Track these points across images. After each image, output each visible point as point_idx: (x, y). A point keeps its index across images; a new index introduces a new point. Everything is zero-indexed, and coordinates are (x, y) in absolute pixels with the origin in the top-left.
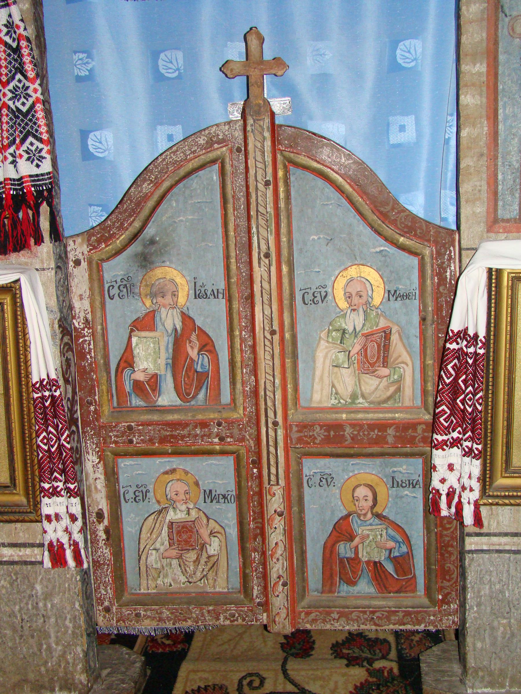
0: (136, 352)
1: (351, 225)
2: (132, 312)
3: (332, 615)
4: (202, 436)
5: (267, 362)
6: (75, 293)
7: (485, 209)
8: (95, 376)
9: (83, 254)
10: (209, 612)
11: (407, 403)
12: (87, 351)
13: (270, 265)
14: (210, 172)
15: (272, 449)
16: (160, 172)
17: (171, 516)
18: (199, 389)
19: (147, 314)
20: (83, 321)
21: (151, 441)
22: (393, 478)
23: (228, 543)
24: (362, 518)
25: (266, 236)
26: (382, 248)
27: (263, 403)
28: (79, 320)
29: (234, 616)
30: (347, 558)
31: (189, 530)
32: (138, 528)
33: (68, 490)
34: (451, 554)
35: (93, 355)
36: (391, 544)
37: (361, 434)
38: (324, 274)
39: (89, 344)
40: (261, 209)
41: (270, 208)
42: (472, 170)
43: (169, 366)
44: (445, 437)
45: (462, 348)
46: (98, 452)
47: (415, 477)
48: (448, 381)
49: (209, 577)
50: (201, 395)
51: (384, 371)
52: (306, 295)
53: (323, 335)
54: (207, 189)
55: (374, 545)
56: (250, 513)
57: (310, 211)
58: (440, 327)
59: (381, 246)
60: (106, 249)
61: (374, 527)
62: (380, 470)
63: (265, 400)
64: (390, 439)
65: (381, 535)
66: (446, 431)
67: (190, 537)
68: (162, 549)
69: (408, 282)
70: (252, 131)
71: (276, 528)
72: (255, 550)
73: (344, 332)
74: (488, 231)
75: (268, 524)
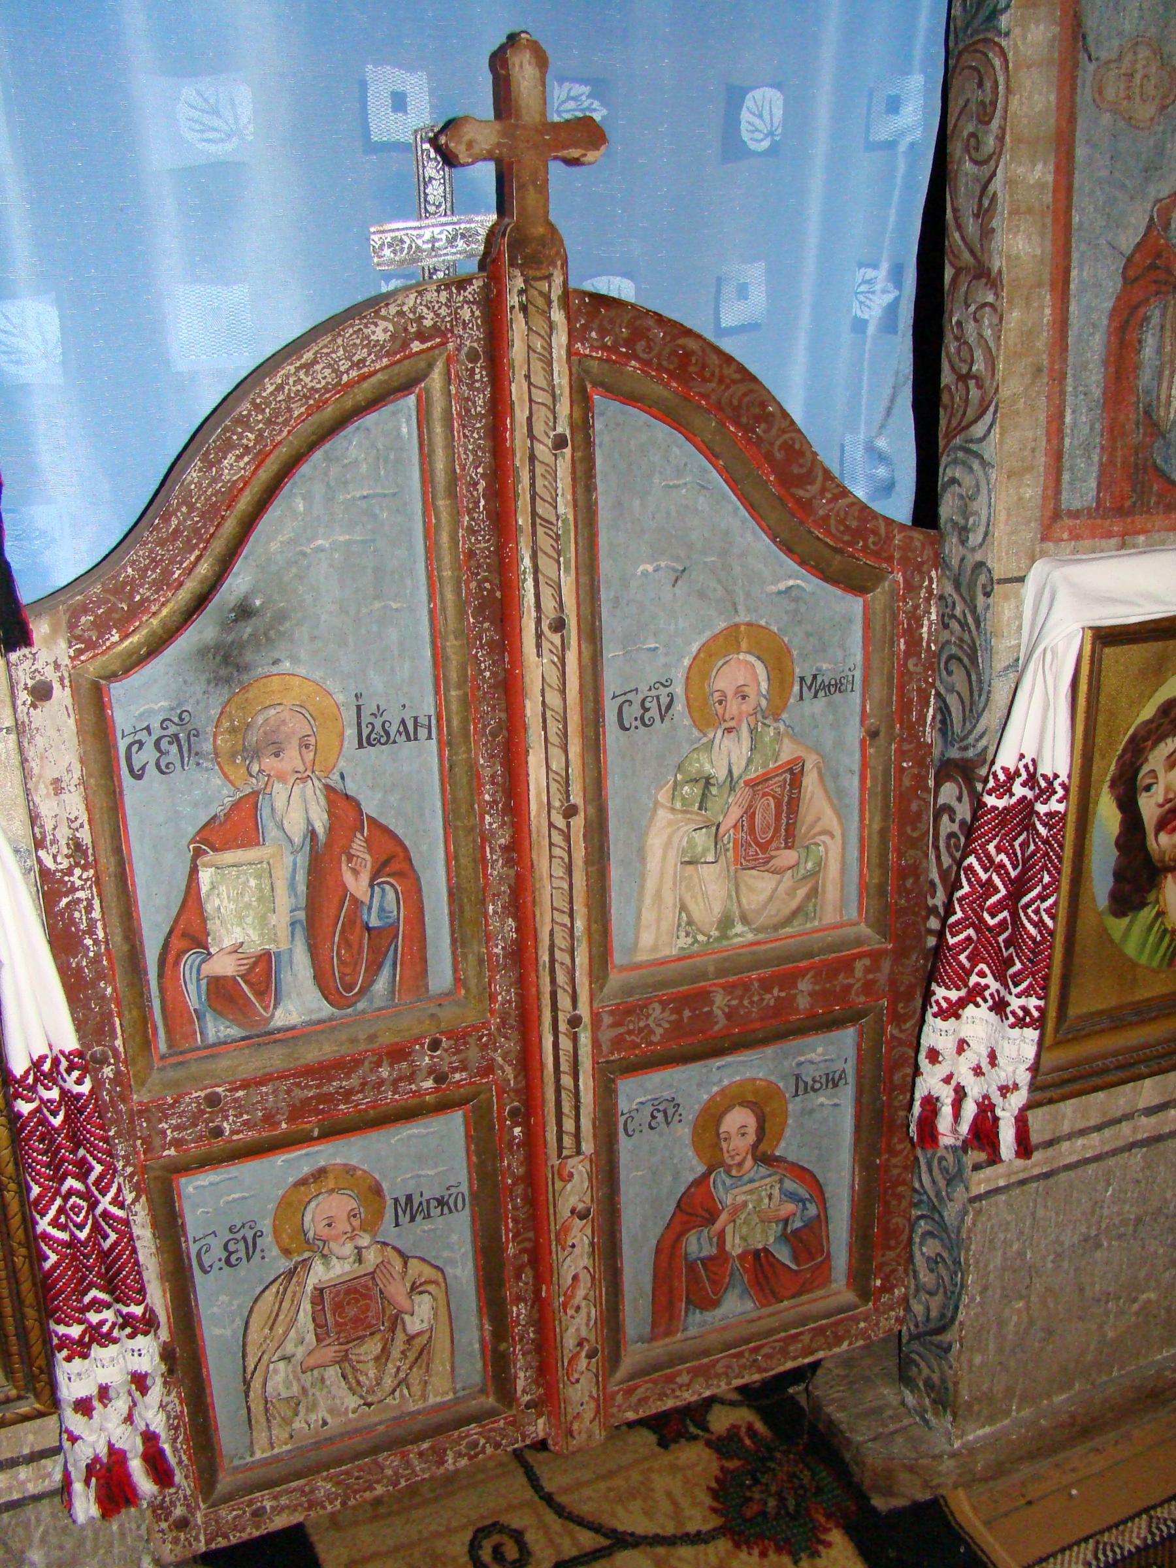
0: (209, 908)
1: (727, 533)
2: (195, 805)
3: (679, 1380)
4: (395, 1083)
5: (556, 883)
6: (40, 776)
7: (1039, 490)
8: (109, 990)
9: (57, 666)
10: (421, 1454)
12: (83, 927)
13: (563, 650)
14: (394, 414)
15: (567, 1081)
16: (269, 422)
17: (319, 1274)
18: (375, 968)
19: (236, 805)
20: (66, 851)
21: (269, 1119)
23: (451, 1297)
24: (734, 1173)
25: (554, 577)
26: (791, 583)
27: (548, 980)
28: (54, 850)
29: (476, 1444)
30: (702, 1260)
31: (362, 1295)
32: (239, 1323)
33: (127, 1320)
35: (101, 934)
37: (746, 1002)
38: (666, 654)
39: (89, 908)
42: (1021, 404)
43: (298, 927)
46: (132, 1175)
49: (411, 1381)
50: (381, 984)
51: (788, 857)
52: (626, 707)
53: (663, 796)
54: (386, 461)
56: (507, 1225)
57: (637, 503)
58: (906, 747)
59: (790, 577)
60: (119, 644)
61: (757, 1184)
62: (772, 1066)
63: (552, 972)
64: (803, 1002)
65: (770, 1197)
68: (300, 1352)
69: (840, 654)
70: (524, 308)
71: (573, 1246)
72: (518, 1299)
73: (708, 781)
74: (1043, 539)
75: (558, 1239)
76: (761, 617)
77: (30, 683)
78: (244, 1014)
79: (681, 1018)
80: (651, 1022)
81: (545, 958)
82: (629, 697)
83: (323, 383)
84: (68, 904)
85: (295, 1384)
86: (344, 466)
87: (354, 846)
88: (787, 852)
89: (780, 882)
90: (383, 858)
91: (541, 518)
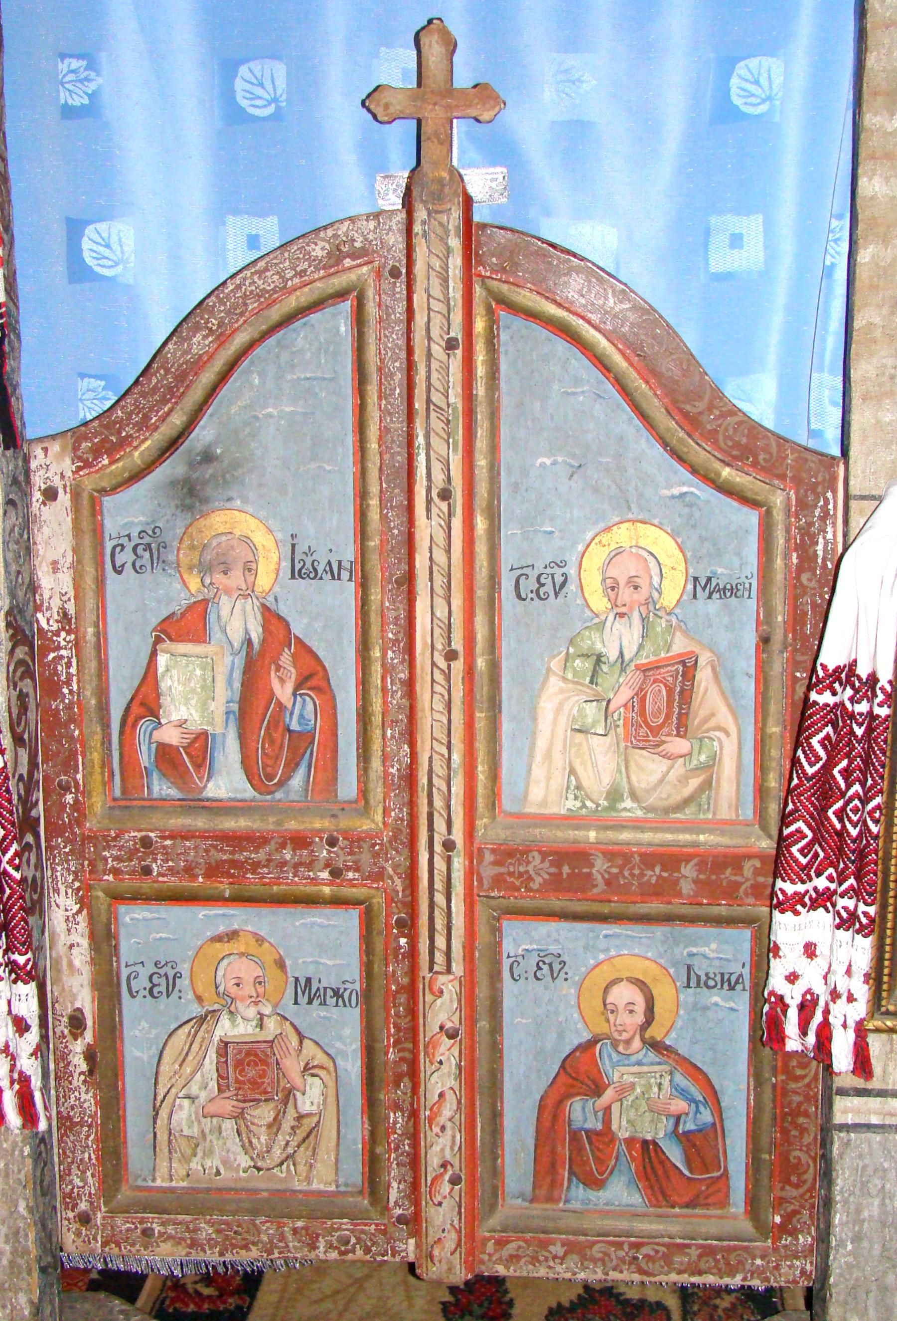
0: (164, 685)
2: (159, 602)
4: (296, 866)
5: (437, 716)
6: (44, 557)
8: (77, 732)
9: (62, 476)
10: (295, 1231)
11: (725, 813)
12: (63, 678)
13: (450, 515)
14: (334, 315)
15: (440, 899)
16: (228, 313)
17: (225, 1028)
18: (292, 766)
19: (190, 608)
20: (56, 617)
21: (189, 871)
22: (689, 967)
23: (341, 1090)
24: (621, 1048)
25: (444, 454)
26: (685, 489)
27: (426, 801)
28: (48, 614)
29: (347, 1242)
30: (587, 1132)
32: (155, 1051)
34: (803, 1130)
35: (75, 687)
36: (679, 1105)
37: (626, 873)
38: (562, 539)
39: (69, 665)
40: (436, 398)
41: (455, 397)
43: (232, 716)
44: (800, 888)
45: (842, 704)
46: (78, 889)
47: (736, 968)
48: (810, 771)
49: (298, 1159)
50: (297, 781)
51: (680, 745)
52: (522, 580)
54: (326, 352)
55: (644, 1107)
57: (537, 405)
59: (684, 484)
61: (645, 1069)
62: (662, 950)
64: (686, 887)
65: (660, 1085)
66: (804, 873)
67: (263, 1075)
68: (203, 1096)
69: (736, 561)
71: (441, 1063)
72: (396, 1107)
73: (599, 659)
76: (655, 517)
77: (43, 487)
78: (181, 777)
79: (561, 873)
80: (530, 868)
81: (425, 781)
82: (525, 571)
83: (272, 286)
84: (54, 658)
85: (196, 1124)
86: (293, 353)
87: (282, 658)
88: (678, 739)
89: (670, 768)
90: (307, 673)
91: (435, 405)
